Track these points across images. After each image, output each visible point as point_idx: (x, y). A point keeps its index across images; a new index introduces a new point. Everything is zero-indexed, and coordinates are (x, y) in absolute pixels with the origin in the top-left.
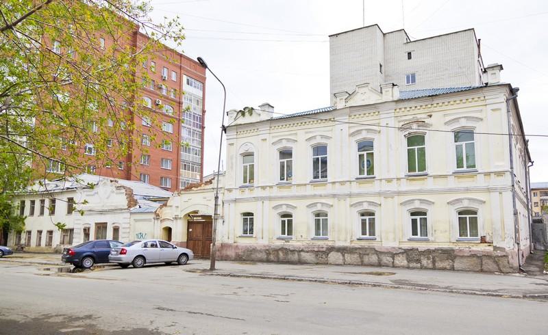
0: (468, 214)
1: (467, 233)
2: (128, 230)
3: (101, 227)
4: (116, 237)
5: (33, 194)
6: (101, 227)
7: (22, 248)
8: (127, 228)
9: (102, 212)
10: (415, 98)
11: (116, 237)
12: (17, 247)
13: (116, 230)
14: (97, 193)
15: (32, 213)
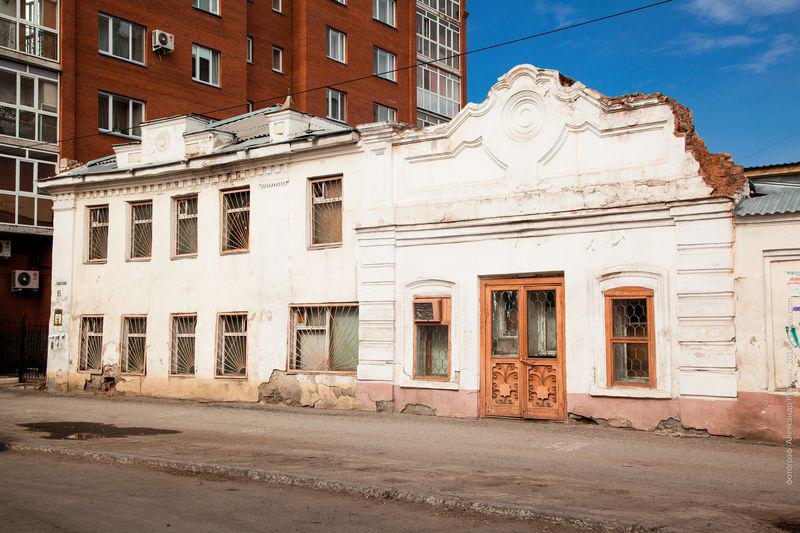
0: (19, 156)
1: (21, 118)
2: (725, 308)
3: (526, 304)
4: (632, 359)
5: (136, 178)
6: (526, 304)
7: (111, 381)
8: (717, 295)
9: (523, 227)
10: (767, 215)
11: (632, 359)
12: (86, 375)
13: (631, 313)
14: (477, 143)
15: (98, 248)
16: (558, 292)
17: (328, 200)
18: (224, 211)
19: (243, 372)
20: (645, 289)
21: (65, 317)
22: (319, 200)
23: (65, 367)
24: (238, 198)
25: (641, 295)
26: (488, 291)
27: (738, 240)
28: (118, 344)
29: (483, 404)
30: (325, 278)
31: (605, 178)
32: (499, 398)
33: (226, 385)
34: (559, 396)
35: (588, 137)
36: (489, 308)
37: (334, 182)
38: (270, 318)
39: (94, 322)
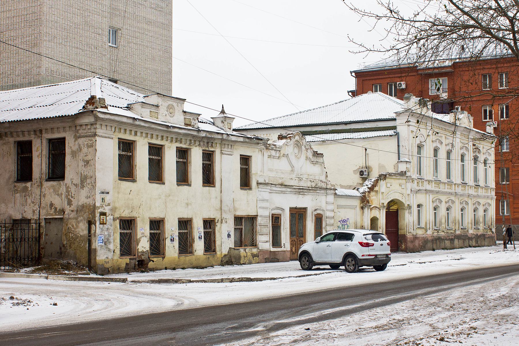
9: (301, 191)
21: (110, 218)
23: (110, 255)
24: (208, 157)
28: (148, 237)
30: (247, 203)
38: (226, 222)
39: (128, 224)
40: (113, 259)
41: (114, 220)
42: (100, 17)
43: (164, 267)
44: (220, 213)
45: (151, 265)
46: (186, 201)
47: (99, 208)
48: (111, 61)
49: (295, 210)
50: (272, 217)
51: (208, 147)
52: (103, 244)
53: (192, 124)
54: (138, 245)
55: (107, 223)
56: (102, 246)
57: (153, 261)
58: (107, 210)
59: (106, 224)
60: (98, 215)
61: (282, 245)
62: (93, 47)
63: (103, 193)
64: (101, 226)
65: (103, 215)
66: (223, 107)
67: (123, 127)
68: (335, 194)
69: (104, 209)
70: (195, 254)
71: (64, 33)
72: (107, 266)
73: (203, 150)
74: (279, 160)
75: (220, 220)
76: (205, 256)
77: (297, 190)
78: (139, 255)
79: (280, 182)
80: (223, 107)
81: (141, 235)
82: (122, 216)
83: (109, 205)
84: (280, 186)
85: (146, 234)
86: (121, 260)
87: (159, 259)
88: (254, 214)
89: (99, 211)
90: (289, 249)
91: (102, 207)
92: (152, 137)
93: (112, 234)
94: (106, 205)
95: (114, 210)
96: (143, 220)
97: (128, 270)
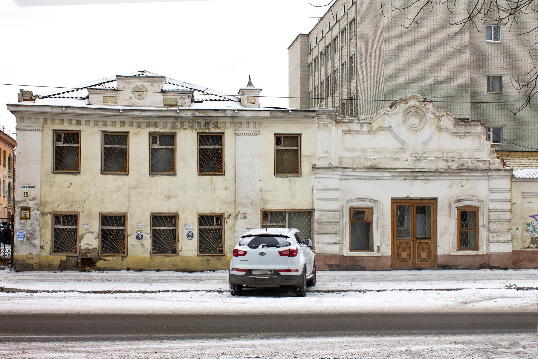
2: (508, 216)
8: (504, 212)
9: (417, 174)
16: (432, 206)
17: (284, 148)
18: (187, 269)
19: (221, 251)
20: (475, 207)
21: (36, 213)
22: (280, 148)
23: (35, 252)
25: (474, 209)
26: (395, 205)
27: (513, 188)
29: (393, 263)
30: (287, 194)
31: (456, 155)
32: (400, 259)
33: (208, 260)
34: (432, 257)
35: (444, 134)
36: (396, 214)
37: (295, 139)
40: (39, 256)
41: (43, 214)
42: (457, 16)
43: (126, 267)
44: (234, 207)
45: (100, 264)
46: (167, 193)
47: (19, 202)
48: (493, 58)
49: (408, 201)
50: (350, 210)
51: (208, 128)
52: (25, 240)
53: (179, 103)
54: (80, 241)
55: (31, 218)
56: (22, 242)
57: (105, 260)
58: (31, 204)
59: (29, 219)
60: (18, 210)
61: (375, 248)
62: (448, 47)
63: (26, 187)
64: (23, 221)
65: (25, 210)
66: (250, 79)
67: (58, 118)
68: (513, 176)
69: (27, 204)
70: (180, 254)
71: (410, 40)
72: (31, 262)
73: (198, 133)
74: (371, 136)
75: (233, 215)
76: (200, 258)
77: (409, 174)
78: (83, 252)
79: (368, 164)
80: (250, 79)
81: (85, 231)
82: (56, 210)
83: (34, 199)
84: (364, 170)
85: (92, 230)
86: (52, 257)
87: (118, 258)
88: (310, 207)
89: (20, 205)
90: (389, 254)
91: (25, 201)
92: (105, 124)
93: (38, 229)
94: (30, 200)
95: (41, 204)
96: (89, 216)
97: (63, 267)
